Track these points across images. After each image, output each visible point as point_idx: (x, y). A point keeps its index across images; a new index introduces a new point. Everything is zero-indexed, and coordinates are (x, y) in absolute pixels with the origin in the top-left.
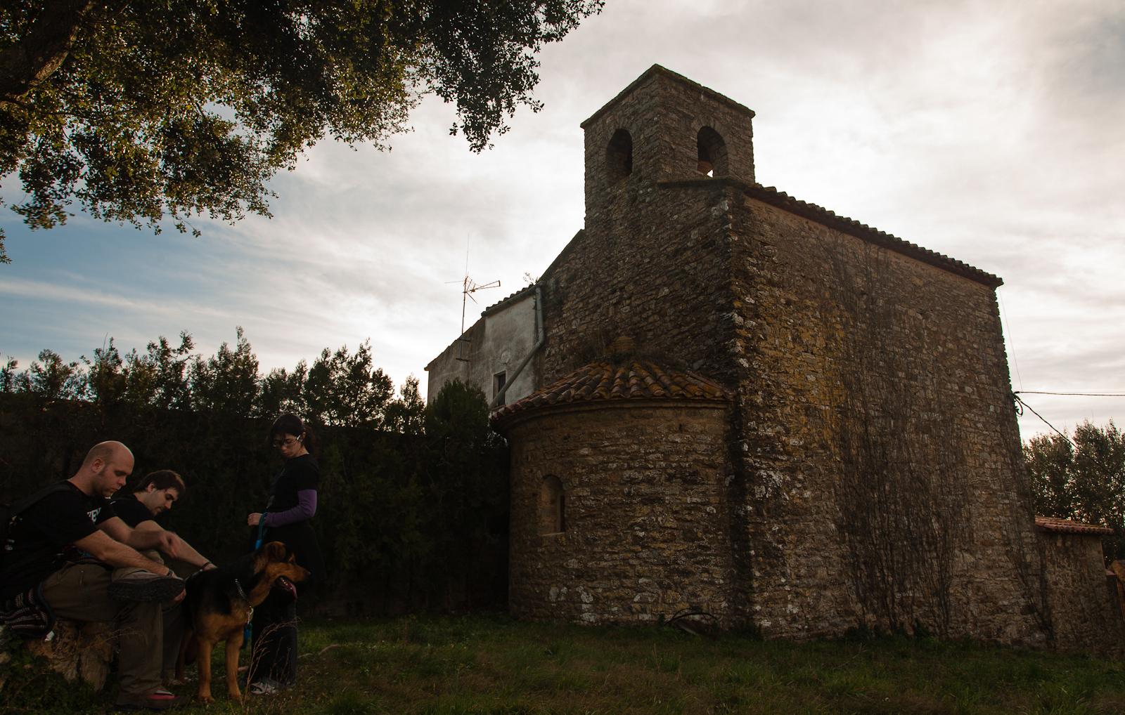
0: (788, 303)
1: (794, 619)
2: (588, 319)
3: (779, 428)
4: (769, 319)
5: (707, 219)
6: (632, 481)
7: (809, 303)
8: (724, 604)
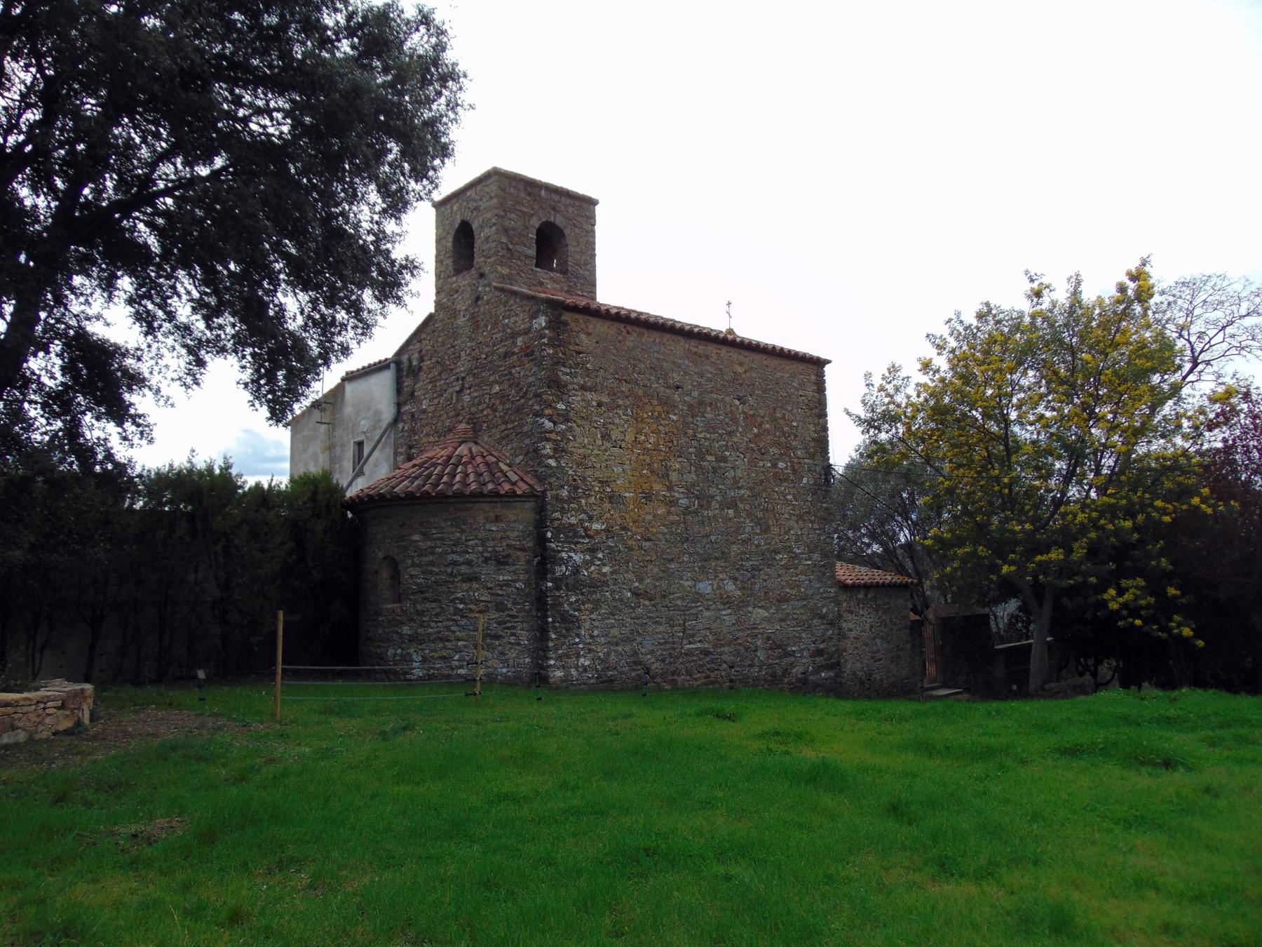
0: (600, 405)
1: (585, 669)
2: (436, 401)
3: (583, 516)
4: (579, 422)
5: (530, 329)
6: (454, 563)
7: (621, 402)
8: (527, 660)
